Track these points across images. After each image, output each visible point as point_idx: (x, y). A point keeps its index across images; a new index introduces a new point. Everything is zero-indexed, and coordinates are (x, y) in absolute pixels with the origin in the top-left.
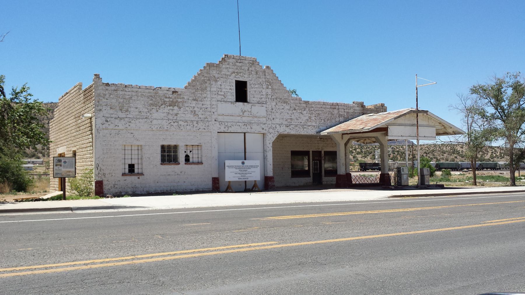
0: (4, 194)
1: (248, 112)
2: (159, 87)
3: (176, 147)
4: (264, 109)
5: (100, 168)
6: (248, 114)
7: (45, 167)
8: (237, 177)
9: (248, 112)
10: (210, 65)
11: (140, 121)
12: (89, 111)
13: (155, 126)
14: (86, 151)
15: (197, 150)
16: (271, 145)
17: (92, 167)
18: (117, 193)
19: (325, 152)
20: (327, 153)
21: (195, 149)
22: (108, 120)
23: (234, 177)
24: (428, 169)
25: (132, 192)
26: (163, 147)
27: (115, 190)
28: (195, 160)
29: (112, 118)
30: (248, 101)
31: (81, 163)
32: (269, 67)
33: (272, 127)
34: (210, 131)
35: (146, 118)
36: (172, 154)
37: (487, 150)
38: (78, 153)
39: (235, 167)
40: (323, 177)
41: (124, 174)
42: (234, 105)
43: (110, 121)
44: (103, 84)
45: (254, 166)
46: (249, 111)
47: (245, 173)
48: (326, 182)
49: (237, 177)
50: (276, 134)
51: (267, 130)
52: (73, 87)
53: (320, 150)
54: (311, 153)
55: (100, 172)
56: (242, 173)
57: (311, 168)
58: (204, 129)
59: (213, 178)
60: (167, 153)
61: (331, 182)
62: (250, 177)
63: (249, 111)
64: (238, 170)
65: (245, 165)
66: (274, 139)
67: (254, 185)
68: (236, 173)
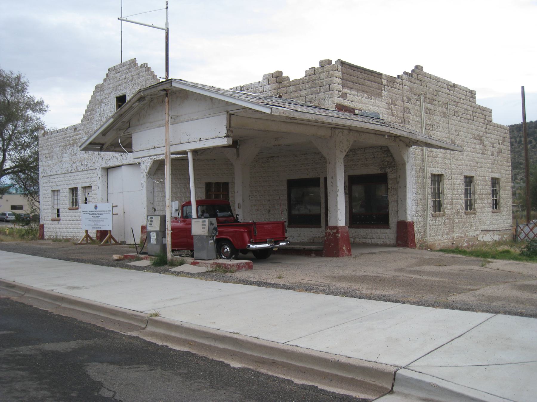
0: (496, 240)
17: (44, 192)
24: (205, 221)
27: (494, 235)
37: (422, 173)
39: (89, 212)
40: (287, 220)
45: (107, 211)
52: (156, 83)
61: (364, 240)
64: (91, 217)
68: (90, 220)
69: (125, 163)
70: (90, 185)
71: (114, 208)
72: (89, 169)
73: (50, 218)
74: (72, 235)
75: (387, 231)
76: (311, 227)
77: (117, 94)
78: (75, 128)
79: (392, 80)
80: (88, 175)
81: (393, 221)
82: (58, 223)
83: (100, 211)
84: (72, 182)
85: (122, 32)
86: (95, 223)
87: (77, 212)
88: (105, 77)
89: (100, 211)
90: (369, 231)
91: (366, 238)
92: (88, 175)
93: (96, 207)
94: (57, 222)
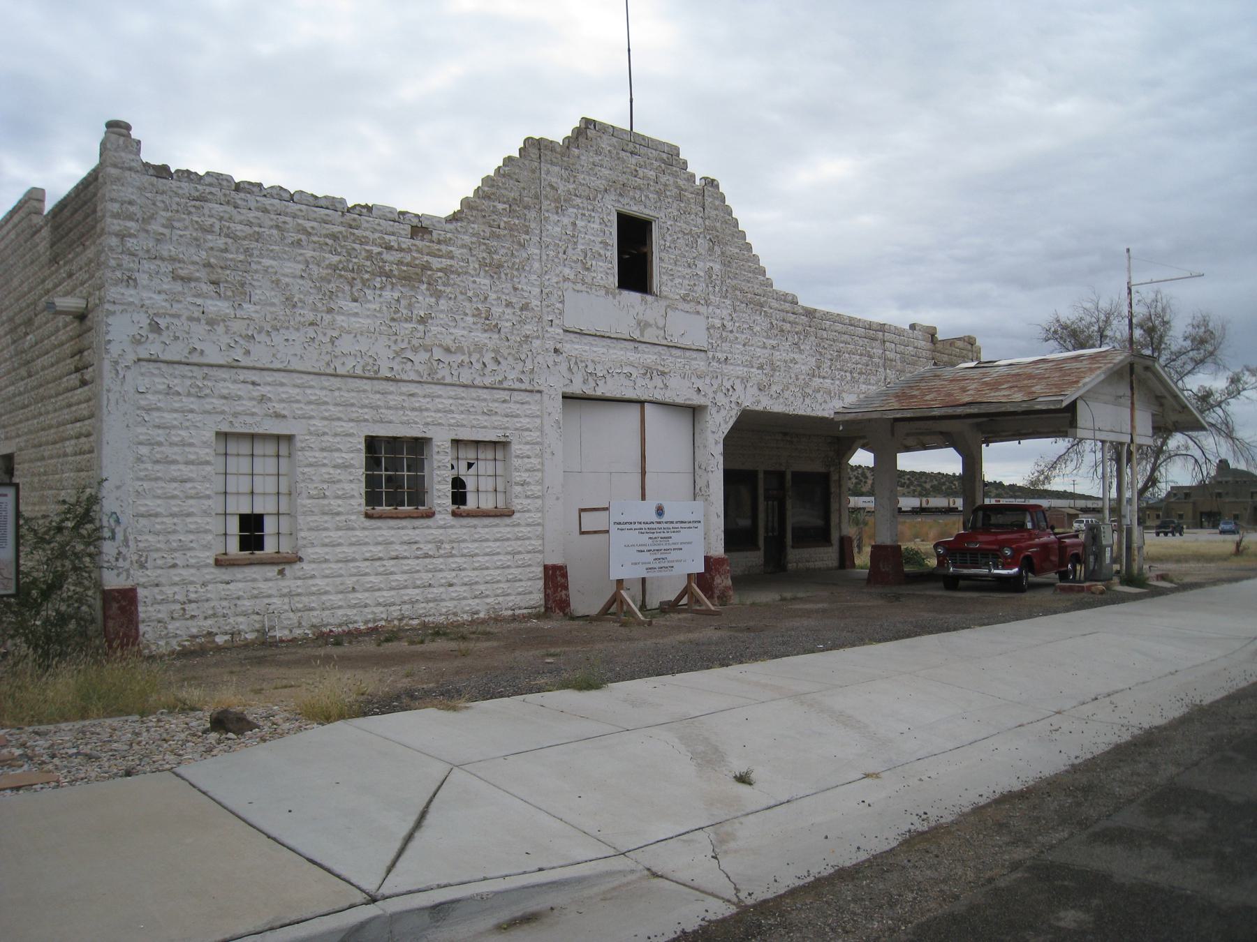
1: (658, 327)
2: (363, 204)
3: (419, 445)
4: (701, 323)
5: (125, 531)
6: (657, 337)
7: (37, 753)
8: (643, 563)
9: (658, 327)
10: (535, 147)
11: (291, 338)
12: (56, 286)
13: (344, 359)
14: (59, 457)
15: (276, 459)
16: (720, 448)
18: (194, 637)
19: (795, 474)
20: (800, 477)
21: (235, 452)
22: (162, 323)
23: (636, 564)
25: (258, 631)
26: (372, 444)
28: (487, 503)
29: (178, 316)
30: (655, 290)
31: (34, 504)
32: (715, 183)
33: (723, 388)
34: (538, 388)
35: (312, 324)
36: (405, 473)
38: (26, 466)
41: (221, 562)
42: (616, 302)
43: (167, 328)
44: (147, 165)
45: (690, 522)
46: (661, 324)
47: (668, 547)
48: (795, 564)
49: (643, 563)
50: (735, 412)
51: (711, 395)
53: (783, 468)
54: (761, 476)
55: (124, 550)
56: (656, 548)
57: (761, 524)
58: (521, 381)
59: (546, 568)
60: (386, 470)
62: (677, 561)
63: (661, 324)
64: (644, 539)
65: (665, 518)
66: (726, 428)
67: (686, 587)
69: (659, 396)
70: (503, 439)
71: (582, 514)
72: (505, 385)
73: (209, 556)
74: (395, 612)
75: (830, 549)
76: (747, 551)
77: (627, 207)
78: (420, 228)
79: (101, 163)
80: (494, 406)
81: (835, 537)
82: (281, 572)
83: (672, 522)
84: (389, 414)
85: (629, 50)
86: (655, 557)
87: (428, 527)
88: (559, 132)
89: (672, 522)
90: (811, 550)
91: (809, 562)
92: (494, 406)
93: (660, 511)
94: (276, 569)
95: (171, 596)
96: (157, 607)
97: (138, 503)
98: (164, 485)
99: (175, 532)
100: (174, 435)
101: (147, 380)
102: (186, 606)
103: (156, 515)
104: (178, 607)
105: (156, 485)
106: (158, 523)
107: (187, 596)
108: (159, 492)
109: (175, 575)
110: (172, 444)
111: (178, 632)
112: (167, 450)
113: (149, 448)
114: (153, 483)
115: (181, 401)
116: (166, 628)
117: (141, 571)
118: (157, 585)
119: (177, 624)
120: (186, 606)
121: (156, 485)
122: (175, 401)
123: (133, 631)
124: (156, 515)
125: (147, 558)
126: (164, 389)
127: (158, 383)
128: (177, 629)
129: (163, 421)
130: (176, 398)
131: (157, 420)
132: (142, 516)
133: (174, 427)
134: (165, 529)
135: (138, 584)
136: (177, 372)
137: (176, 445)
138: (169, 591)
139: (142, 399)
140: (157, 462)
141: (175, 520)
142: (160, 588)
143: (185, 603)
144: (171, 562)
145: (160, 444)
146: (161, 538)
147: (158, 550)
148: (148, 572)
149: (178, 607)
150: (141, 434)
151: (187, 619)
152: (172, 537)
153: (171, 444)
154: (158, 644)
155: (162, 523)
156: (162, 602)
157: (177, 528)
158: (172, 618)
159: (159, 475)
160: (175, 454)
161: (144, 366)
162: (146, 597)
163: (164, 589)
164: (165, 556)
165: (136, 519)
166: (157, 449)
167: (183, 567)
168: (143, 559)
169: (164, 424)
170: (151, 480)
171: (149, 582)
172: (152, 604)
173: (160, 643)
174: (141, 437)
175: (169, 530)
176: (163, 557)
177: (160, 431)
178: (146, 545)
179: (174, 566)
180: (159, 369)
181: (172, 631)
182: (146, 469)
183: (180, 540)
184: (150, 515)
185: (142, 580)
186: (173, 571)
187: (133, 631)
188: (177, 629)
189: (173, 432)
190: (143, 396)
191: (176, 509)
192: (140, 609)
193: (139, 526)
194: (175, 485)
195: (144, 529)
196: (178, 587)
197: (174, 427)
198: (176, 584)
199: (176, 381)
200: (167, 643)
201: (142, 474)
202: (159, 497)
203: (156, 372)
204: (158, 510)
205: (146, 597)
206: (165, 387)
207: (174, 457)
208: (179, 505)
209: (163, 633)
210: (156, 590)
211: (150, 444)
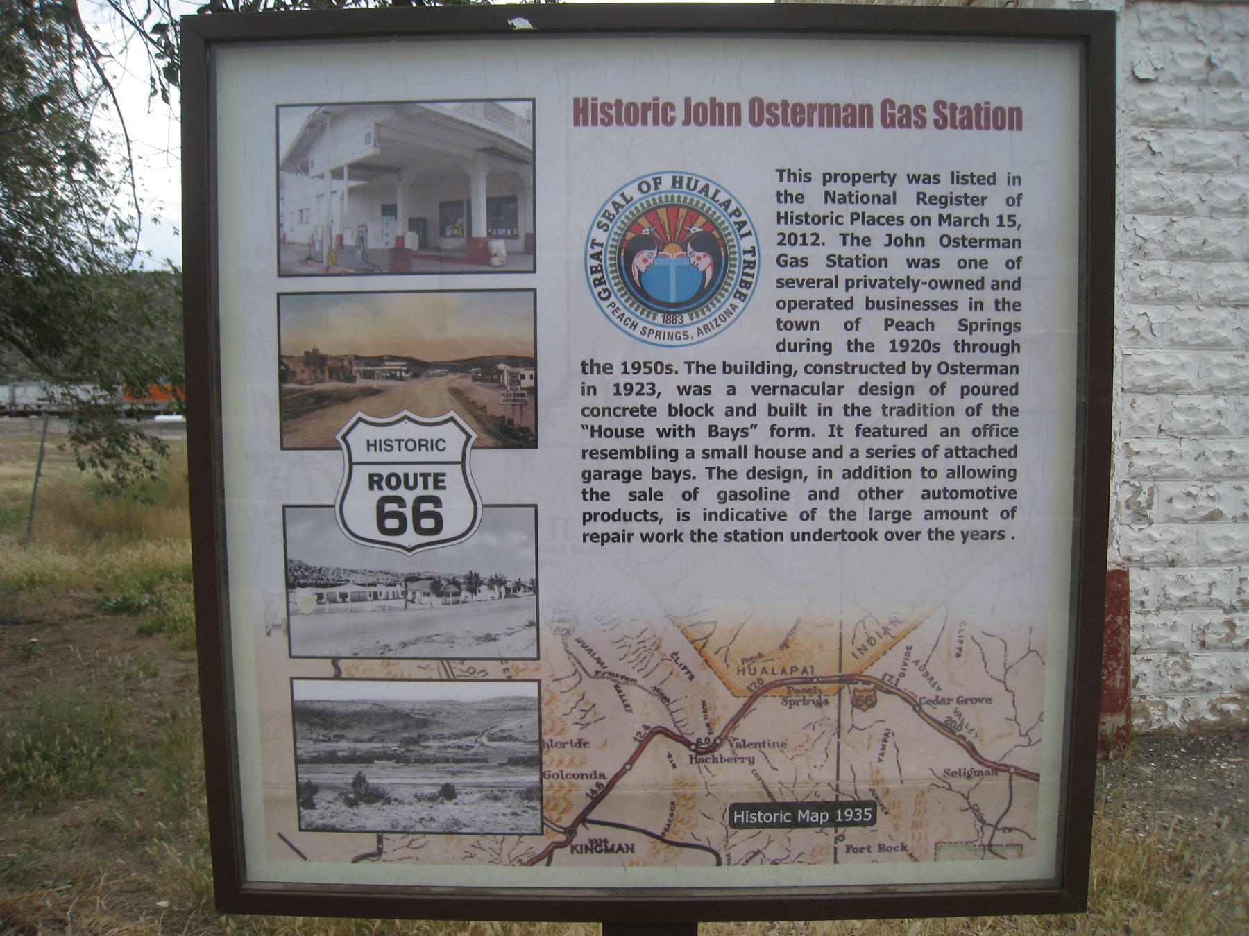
95: (1203, 590)
96: (1169, 616)
97: (1137, 358)
98: (1195, 313)
99: (1218, 431)
100: (1221, 187)
101: (1156, 50)
102: (1236, 617)
103: (1177, 389)
104: (1218, 617)
105: (1177, 315)
106: (1179, 410)
107: (1240, 591)
108: (1185, 331)
109: (1215, 539)
110: (1214, 211)
111: (1214, 679)
112: (1203, 226)
113: (1162, 220)
114: (1170, 309)
115: (1238, 99)
116: (1187, 668)
117: (1136, 527)
118: (1172, 563)
119: (1213, 659)
120: (1236, 617)
121: (1177, 315)
122: (1223, 101)
123: (1119, 676)
124: (1177, 389)
125: (1151, 494)
126: (1198, 71)
127: (1182, 55)
128: (1213, 671)
129: (1195, 152)
130: (1226, 94)
131: (1180, 150)
132: (1145, 391)
133: (1220, 167)
134: (1196, 425)
135: (1129, 559)
136: (1228, 26)
137: (1225, 211)
138: (1199, 578)
139: (1141, 96)
140: (1180, 256)
141: (1220, 402)
142: (1178, 570)
143: (1233, 609)
144: (1206, 507)
145: (1186, 211)
146: (1186, 446)
147: (1177, 476)
148: (1153, 531)
149: (1218, 617)
150: (1143, 185)
151: (1235, 649)
152: (1214, 446)
153: (1213, 209)
154: (1166, 706)
155: (1191, 408)
156: (1186, 603)
157: (1223, 422)
158: (1203, 644)
159: (1185, 287)
160: (1224, 235)
161: (1148, 13)
162: (1146, 592)
163: (1187, 572)
164: (1194, 491)
165: (1129, 397)
166: (1182, 223)
167: (1235, 520)
168: (1143, 498)
169: (1198, 159)
170: (1163, 301)
171: (1154, 554)
172: (1158, 609)
173: (1170, 703)
174: (1143, 194)
175: (1206, 427)
176: (1189, 494)
177: (1188, 179)
178: (1151, 462)
179: (1214, 517)
180: (1185, 19)
181: (1199, 675)
182: (1155, 274)
183: (1231, 453)
184: (1161, 390)
185: (1139, 550)
186: (1210, 530)
187: (1119, 676)
188: (1213, 671)
189: (1218, 180)
190: (1145, 90)
191: (1222, 376)
192: (1135, 619)
193: (1136, 417)
194: (1223, 313)
195: (1149, 425)
196: (1220, 569)
197: (1220, 167)
198: (1216, 562)
199: (1226, 49)
200: (1187, 705)
201: (1148, 285)
202: (1184, 345)
203: (1178, 27)
204: (1182, 376)
205: (1146, 592)
206: (1200, 64)
207: (1221, 243)
208: (1231, 364)
209: (1178, 680)
210: (1169, 575)
211: (1166, 211)
